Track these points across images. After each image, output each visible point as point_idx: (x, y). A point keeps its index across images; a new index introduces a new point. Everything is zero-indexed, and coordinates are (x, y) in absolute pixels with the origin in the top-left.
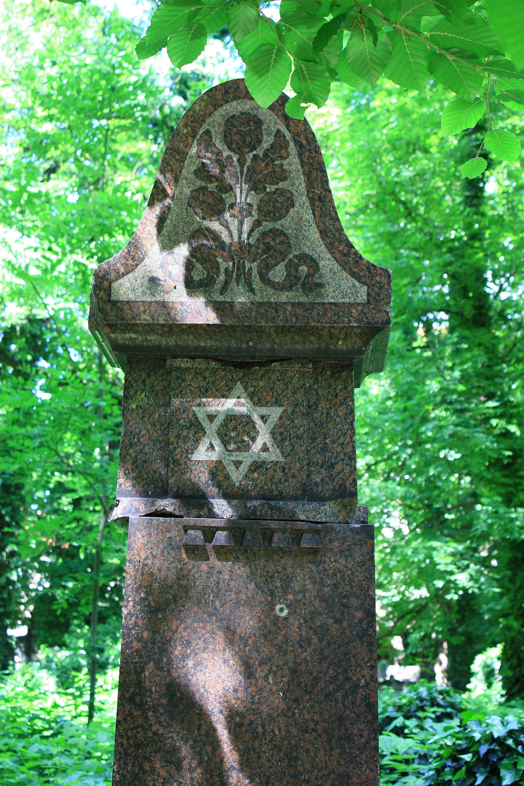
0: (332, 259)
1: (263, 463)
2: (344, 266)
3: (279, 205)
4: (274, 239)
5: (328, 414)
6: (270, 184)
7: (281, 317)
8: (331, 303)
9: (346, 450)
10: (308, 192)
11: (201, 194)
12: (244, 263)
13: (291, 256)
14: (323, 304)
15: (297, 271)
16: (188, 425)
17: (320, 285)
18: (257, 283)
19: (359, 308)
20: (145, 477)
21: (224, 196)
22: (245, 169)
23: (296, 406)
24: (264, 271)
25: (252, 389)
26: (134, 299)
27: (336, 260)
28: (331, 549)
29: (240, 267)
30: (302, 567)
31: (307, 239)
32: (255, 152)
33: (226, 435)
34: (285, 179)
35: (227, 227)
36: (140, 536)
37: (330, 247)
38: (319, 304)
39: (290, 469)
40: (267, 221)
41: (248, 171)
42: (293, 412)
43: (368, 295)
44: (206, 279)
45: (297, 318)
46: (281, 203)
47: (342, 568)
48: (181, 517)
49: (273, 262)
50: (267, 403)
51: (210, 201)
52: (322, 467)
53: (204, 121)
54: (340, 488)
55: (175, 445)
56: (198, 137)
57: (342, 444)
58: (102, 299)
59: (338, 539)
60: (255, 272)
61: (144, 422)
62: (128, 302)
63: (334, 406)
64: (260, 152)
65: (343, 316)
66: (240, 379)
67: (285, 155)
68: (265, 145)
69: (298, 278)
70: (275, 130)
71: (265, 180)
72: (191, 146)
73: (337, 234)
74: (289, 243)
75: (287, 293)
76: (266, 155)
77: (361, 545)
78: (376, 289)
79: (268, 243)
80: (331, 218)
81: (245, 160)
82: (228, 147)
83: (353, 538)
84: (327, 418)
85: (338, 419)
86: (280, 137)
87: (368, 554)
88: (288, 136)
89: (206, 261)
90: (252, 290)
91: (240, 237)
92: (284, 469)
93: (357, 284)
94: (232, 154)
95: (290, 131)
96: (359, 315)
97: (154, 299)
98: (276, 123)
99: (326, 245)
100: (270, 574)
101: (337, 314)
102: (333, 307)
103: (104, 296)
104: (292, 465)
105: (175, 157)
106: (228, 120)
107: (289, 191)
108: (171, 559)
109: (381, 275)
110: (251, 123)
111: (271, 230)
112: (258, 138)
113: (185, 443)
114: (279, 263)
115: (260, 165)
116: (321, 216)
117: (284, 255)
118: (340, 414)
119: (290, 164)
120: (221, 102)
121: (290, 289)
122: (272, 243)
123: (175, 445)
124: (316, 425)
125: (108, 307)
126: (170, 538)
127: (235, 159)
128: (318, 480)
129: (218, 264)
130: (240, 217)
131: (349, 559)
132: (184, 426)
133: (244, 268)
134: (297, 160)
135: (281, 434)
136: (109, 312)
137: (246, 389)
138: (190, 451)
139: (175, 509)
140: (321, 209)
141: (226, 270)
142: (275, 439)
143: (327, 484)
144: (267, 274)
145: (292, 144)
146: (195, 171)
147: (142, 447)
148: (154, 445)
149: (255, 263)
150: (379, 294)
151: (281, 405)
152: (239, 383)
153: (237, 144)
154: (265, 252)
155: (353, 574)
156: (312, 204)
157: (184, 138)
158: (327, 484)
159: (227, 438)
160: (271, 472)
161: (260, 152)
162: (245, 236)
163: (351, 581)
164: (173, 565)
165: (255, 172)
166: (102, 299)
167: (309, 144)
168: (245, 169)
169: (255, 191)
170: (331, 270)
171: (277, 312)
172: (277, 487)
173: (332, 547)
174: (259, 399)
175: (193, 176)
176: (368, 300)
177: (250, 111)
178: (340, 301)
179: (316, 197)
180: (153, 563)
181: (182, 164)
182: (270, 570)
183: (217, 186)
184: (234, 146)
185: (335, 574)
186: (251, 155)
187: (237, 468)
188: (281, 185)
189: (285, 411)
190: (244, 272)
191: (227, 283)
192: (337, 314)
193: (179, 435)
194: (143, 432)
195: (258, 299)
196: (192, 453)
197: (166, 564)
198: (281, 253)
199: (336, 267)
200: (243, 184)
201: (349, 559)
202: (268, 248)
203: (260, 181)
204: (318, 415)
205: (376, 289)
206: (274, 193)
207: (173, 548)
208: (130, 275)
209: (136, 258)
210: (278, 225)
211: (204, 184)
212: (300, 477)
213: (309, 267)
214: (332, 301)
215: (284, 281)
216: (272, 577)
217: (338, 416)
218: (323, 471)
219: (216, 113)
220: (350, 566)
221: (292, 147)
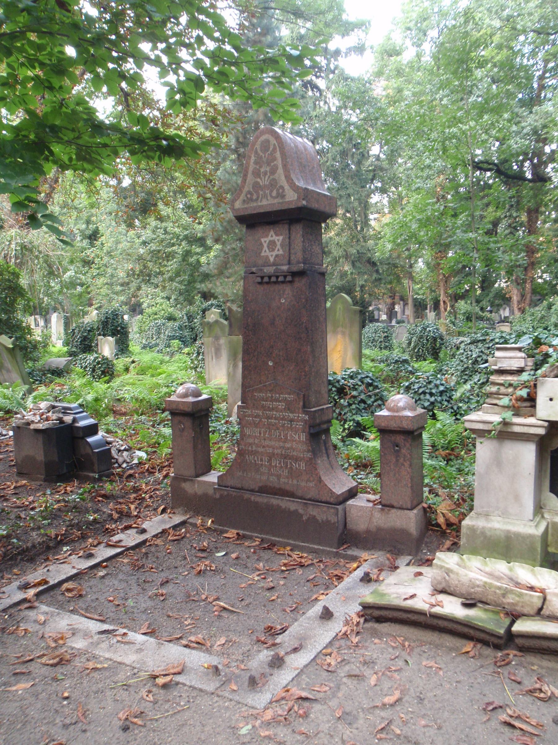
2: (291, 187)
17: (285, 196)
18: (269, 198)
37: (288, 181)
64: (269, 152)
68: (271, 149)
117: (276, 186)
161: (269, 152)
202: (272, 185)
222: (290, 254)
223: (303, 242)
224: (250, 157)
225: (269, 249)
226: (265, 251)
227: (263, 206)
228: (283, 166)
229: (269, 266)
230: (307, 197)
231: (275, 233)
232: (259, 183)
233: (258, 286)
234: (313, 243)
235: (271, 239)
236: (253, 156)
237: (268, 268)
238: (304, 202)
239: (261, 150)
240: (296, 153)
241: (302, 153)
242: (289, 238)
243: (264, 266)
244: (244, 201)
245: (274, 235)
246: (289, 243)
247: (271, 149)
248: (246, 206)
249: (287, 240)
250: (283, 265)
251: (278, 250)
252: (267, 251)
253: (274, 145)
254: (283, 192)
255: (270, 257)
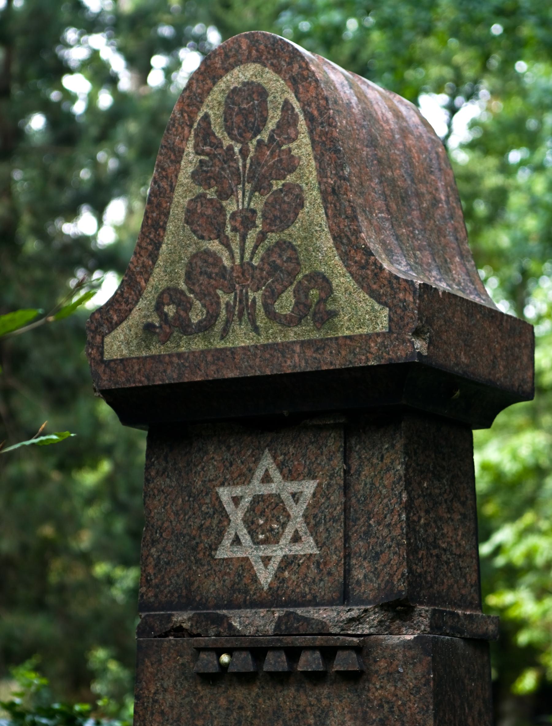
0: (348, 274)
1: (295, 557)
2: (361, 281)
3: (285, 206)
4: (280, 256)
5: (372, 484)
6: (276, 179)
7: (289, 363)
8: (346, 337)
9: (394, 534)
10: (320, 184)
11: (199, 204)
12: (247, 293)
13: (300, 276)
14: (337, 339)
15: (307, 296)
16: (211, 511)
17: (334, 314)
18: (261, 321)
19: (379, 340)
20: (168, 583)
21: (224, 203)
22: (248, 161)
23: (332, 477)
24: (269, 301)
25: (281, 458)
26: (128, 356)
27: (352, 275)
28: (377, 672)
29: (243, 299)
30: (340, 698)
31: (318, 249)
32: (259, 137)
33: (253, 522)
34: (291, 171)
35: (228, 246)
36: (149, 664)
37: (345, 257)
38: (331, 339)
39: (325, 563)
40: (272, 231)
41: (251, 165)
42: (329, 485)
43: (390, 320)
44: (205, 320)
45: (307, 363)
46: (288, 203)
47: (390, 697)
48: (199, 635)
49: (279, 287)
50: (299, 475)
51: (209, 212)
52: (365, 558)
53: (202, 102)
54: (386, 585)
55: (198, 540)
56: (195, 125)
57: (389, 524)
58: (94, 359)
59: (384, 657)
60: (259, 303)
61: (166, 510)
62: (122, 360)
63: (379, 472)
64: (264, 136)
65: (359, 354)
66: (268, 446)
67: (293, 136)
68: (271, 125)
69: (308, 307)
70: (281, 101)
71: (271, 174)
72: (187, 140)
73: (353, 239)
74: (297, 259)
75: (296, 329)
76: (271, 138)
77: (414, 664)
78: (399, 311)
79: (274, 261)
80: (347, 217)
81: (248, 150)
82: (229, 134)
83: (404, 656)
84: (371, 489)
85: (384, 491)
86: (288, 109)
87: (424, 676)
88: (296, 105)
89: (205, 295)
90: (256, 329)
91: (242, 258)
92: (318, 563)
93: (377, 306)
94: (233, 143)
95: (299, 100)
96: (379, 349)
97: (148, 353)
98: (283, 92)
99: (340, 256)
100: (301, 709)
101: (352, 351)
102: (348, 342)
103: (96, 355)
104: (328, 558)
105: (170, 157)
106: (228, 97)
107: (298, 185)
108: (185, 692)
109: (405, 290)
110: (255, 96)
111: (277, 243)
112: (262, 116)
113: (208, 536)
114: (286, 287)
115: (264, 154)
116: (335, 216)
117: (292, 274)
118: (386, 483)
119: (299, 147)
120: (221, 71)
121: (299, 323)
122: (279, 262)
123: (198, 540)
124: (359, 500)
125: (101, 369)
126: (183, 664)
127: (236, 150)
128: (361, 577)
129: (218, 298)
130: (242, 230)
131: (399, 685)
132: (207, 513)
133: (247, 300)
134: (307, 140)
135: (315, 516)
136: (102, 375)
137: (274, 458)
138: (213, 547)
139: (192, 626)
140: (335, 206)
141: (227, 304)
142: (308, 524)
143: (371, 581)
144: (273, 305)
145: (301, 117)
146: (193, 173)
147: (164, 543)
148: (178, 540)
149: (260, 292)
150: (402, 318)
151: (314, 478)
152: (267, 451)
153: (239, 128)
154: (270, 274)
155: (404, 704)
156: (325, 200)
157: (180, 129)
158: (371, 581)
159: (253, 527)
160: (303, 569)
161: (264, 136)
162: (247, 255)
163: (402, 714)
164: (187, 700)
165: (259, 164)
166: (94, 359)
167: (321, 114)
168: (248, 161)
169: (259, 191)
170: (346, 290)
171: (284, 356)
172: (310, 590)
173: (377, 668)
174: (290, 471)
175: (190, 180)
176: (390, 328)
177: (254, 79)
178: (358, 332)
179: (330, 189)
180: (164, 698)
181: (177, 165)
182: (301, 703)
183: (216, 191)
184: (235, 132)
185: (381, 706)
186: (254, 142)
187: (266, 566)
188: (290, 178)
189: (319, 485)
190: (247, 305)
191: (228, 322)
192: (352, 351)
193: (202, 525)
194: (166, 525)
195: (262, 341)
196: (216, 549)
197: (179, 698)
198: (289, 274)
199: (353, 285)
200: (246, 184)
201: (399, 685)
202: (275, 268)
203: (264, 176)
204: (361, 487)
205: (399, 311)
206: (281, 190)
207: (186, 678)
208: (124, 324)
209: (130, 301)
210: (284, 236)
211: (201, 190)
212: (337, 573)
213: (321, 289)
214: (347, 333)
215: (292, 312)
216: (304, 712)
217: (385, 487)
218: (366, 564)
219: (215, 89)
220: (400, 693)
221: (302, 124)
222: (347, 556)
223: (409, 507)
224: (179, 154)
225: (252, 533)
226: (237, 541)
227: (233, 351)
228: (324, 194)
229: (254, 604)
230: (429, 322)
231: (280, 467)
232: (217, 260)
233: (203, 691)
234: (442, 510)
235: (265, 490)
236: (190, 148)
237: (248, 612)
238: (420, 345)
239: (229, 130)
240: (373, 143)
241: (393, 143)
242: (346, 488)
243: (230, 606)
244: (149, 328)
245: (276, 475)
246: (346, 509)
247: (271, 125)
248: (156, 350)
249: (337, 497)
250: (315, 603)
251: (296, 539)
252: (246, 539)
253: (287, 106)
254: (322, 301)
255: (258, 567)
